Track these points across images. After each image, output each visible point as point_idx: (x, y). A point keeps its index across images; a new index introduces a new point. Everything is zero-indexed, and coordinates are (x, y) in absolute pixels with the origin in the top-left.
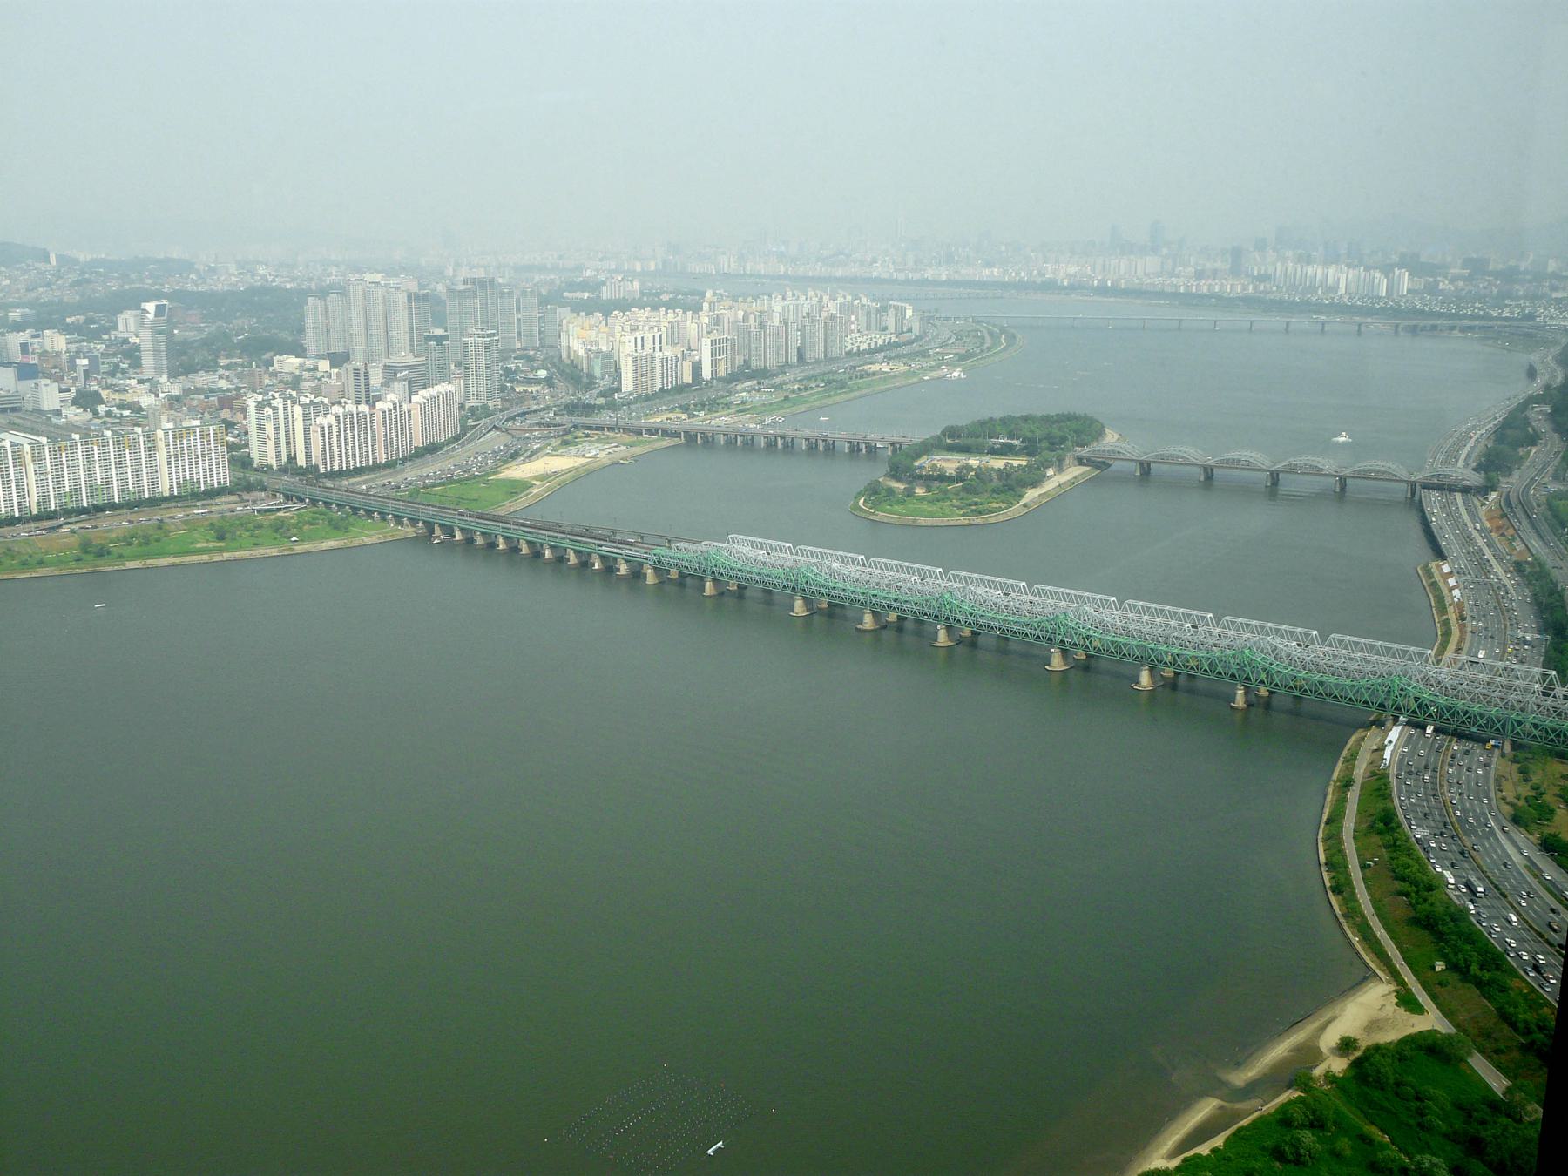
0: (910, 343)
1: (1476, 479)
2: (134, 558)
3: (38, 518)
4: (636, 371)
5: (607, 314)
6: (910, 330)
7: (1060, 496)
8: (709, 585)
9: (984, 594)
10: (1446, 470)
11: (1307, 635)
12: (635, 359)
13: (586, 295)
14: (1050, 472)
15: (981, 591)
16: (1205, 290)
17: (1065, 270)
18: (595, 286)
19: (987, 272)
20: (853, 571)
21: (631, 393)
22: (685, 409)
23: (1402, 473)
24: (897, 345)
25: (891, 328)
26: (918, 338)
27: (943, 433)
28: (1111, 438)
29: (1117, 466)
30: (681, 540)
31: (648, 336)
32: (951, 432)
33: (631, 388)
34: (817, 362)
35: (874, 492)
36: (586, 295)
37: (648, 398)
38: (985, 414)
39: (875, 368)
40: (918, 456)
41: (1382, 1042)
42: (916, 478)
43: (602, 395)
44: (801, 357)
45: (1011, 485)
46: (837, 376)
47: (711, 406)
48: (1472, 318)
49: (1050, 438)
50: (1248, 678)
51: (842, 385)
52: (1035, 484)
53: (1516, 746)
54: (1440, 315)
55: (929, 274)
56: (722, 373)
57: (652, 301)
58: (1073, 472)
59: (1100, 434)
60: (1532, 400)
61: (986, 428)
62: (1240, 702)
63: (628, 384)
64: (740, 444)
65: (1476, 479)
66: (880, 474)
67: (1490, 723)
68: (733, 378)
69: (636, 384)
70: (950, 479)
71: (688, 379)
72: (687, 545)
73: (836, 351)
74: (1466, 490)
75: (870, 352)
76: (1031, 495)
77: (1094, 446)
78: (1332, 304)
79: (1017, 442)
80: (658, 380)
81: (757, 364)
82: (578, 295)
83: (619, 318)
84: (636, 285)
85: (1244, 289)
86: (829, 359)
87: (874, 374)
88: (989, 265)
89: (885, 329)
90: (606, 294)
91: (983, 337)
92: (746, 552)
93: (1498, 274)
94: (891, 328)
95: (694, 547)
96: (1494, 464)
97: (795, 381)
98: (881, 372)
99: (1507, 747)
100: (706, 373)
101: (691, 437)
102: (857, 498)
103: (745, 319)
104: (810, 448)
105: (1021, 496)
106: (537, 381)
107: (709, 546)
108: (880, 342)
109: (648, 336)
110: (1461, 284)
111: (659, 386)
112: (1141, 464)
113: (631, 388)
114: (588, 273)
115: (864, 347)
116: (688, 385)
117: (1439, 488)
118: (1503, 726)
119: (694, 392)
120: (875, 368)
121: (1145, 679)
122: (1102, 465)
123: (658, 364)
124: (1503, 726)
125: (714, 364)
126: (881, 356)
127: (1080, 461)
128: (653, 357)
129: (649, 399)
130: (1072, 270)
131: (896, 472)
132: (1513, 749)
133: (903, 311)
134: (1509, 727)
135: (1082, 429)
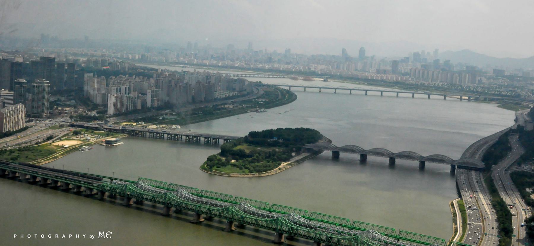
1: (482, 165)
2: (67, 137)
3: (467, 91)
10: (471, 161)
14: (293, 154)
31: (123, 88)
34: (201, 102)
39: (226, 106)
40: (235, 145)
48: (494, 95)
56: (155, 105)
65: (482, 165)
72: (119, 182)
74: (477, 170)
78: (434, 86)
79: (281, 141)
91: (278, 95)
93: (507, 77)
105: (280, 165)
106: (69, 106)
110: (492, 80)
116: (139, 110)
123: (125, 99)
125: (152, 101)
126: (229, 101)
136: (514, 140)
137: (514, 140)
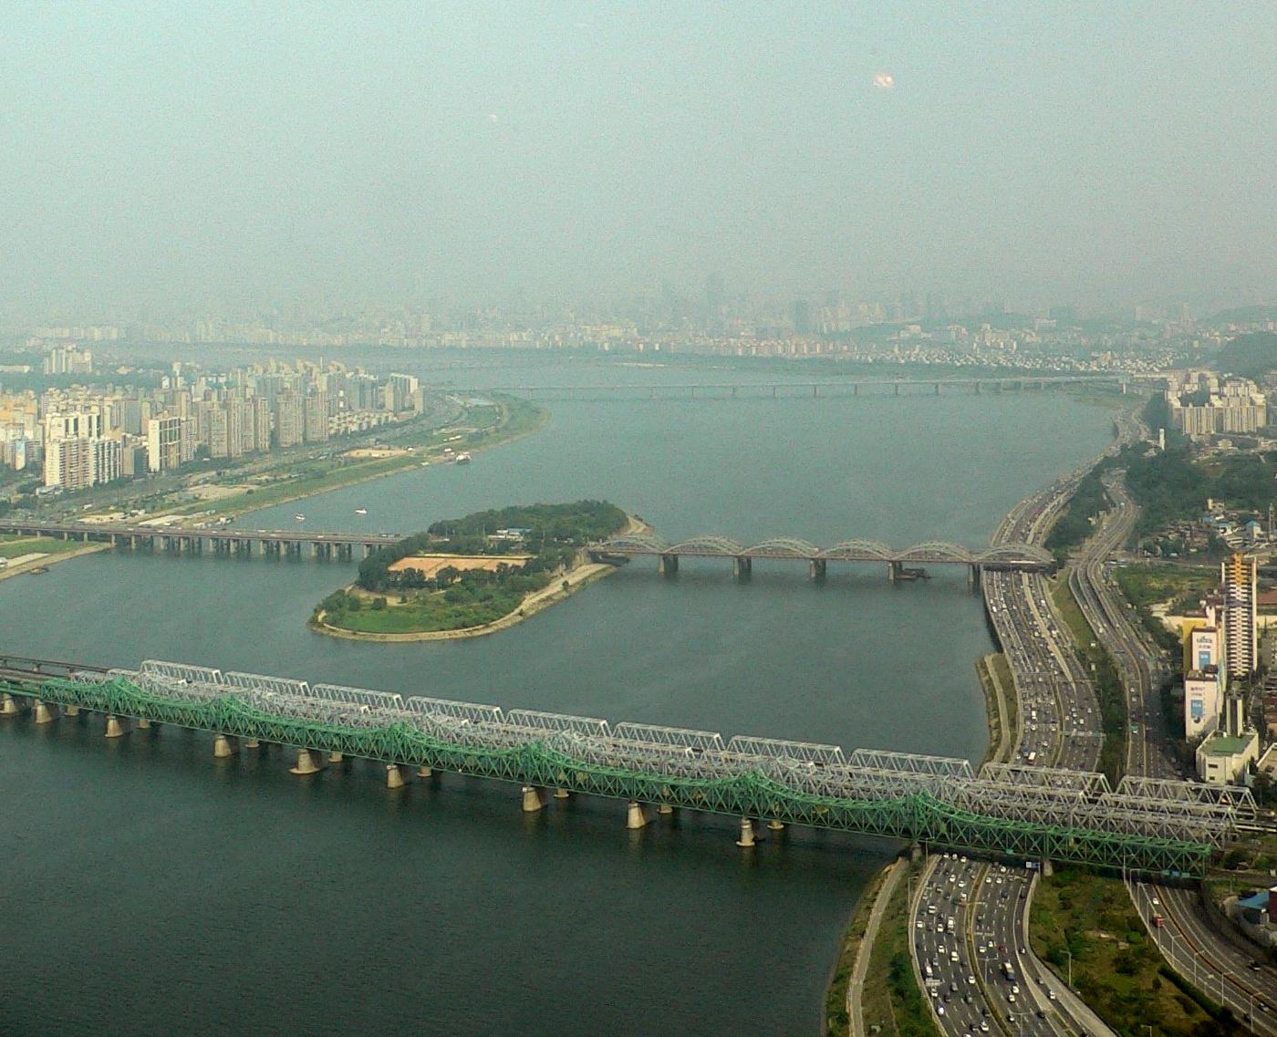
0: (415, 421)
1: (1047, 558)
4: (63, 462)
5: (40, 392)
6: (412, 408)
7: (573, 596)
8: (112, 724)
9: (449, 724)
11: (829, 753)
12: (63, 446)
13: (26, 369)
15: (442, 720)
16: (766, 353)
17: (610, 334)
18: (37, 358)
19: (514, 337)
20: (291, 701)
21: (57, 488)
22: (122, 507)
23: (965, 556)
24: (394, 425)
25: (390, 404)
26: (425, 416)
27: (430, 531)
28: (636, 530)
29: (638, 563)
30: (82, 668)
31: (83, 419)
32: (438, 529)
33: (57, 481)
34: (295, 445)
35: (338, 607)
36: (26, 369)
37: (78, 494)
38: (484, 508)
39: (364, 453)
40: (396, 559)
41: (903, 848)
42: (391, 585)
43: (21, 490)
44: (274, 436)
45: (513, 585)
46: (313, 467)
47: (153, 504)
49: (559, 531)
50: (754, 810)
51: (320, 475)
52: (535, 588)
53: (1058, 867)
54: (1024, 372)
55: (448, 339)
57: (101, 380)
58: (584, 570)
59: (621, 523)
60: (1108, 462)
61: (489, 522)
62: (747, 841)
63: (53, 476)
64: (185, 549)
65: (1047, 558)
66: (347, 582)
67: (1026, 841)
68: (186, 468)
69: (63, 477)
70: (430, 585)
71: (265, 443)
72: (89, 675)
73: (311, 437)
75: (363, 434)
76: (530, 601)
77: (614, 539)
80: (92, 472)
81: (219, 450)
82: (17, 368)
83: (54, 398)
84: (88, 357)
85: (810, 349)
86: (307, 443)
87: (362, 460)
88: (519, 327)
89: (382, 406)
90: (51, 367)
92: (162, 681)
94: (390, 404)
95: (98, 676)
96: (1064, 537)
97: (266, 471)
98: (370, 459)
99: (1048, 871)
100: (154, 463)
101: (123, 540)
102: (317, 611)
103: (207, 397)
104: (269, 551)
107: (116, 675)
108: (374, 422)
109: (83, 419)
111: (91, 479)
112: (665, 557)
113: (57, 481)
114: (32, 342)
115: (354, 428)
117: (1004, 569)
118: (1041, 844)
119: (132, 483)
120: (364, 453)
121: (635, 818)
122: (618, 562)
123: (92, 450)
124: (1041, 844)
125: (164, 451)
127: (594, 557)
128: (85, 443)
129: (72, 495)
130: (617, 332)
131: (366, 582)
132: (1055, 871)
133: (407, 383)
134: (1047, 846)
135: (603, 518)
136: (1114, 484)
137: (1114, 484)
